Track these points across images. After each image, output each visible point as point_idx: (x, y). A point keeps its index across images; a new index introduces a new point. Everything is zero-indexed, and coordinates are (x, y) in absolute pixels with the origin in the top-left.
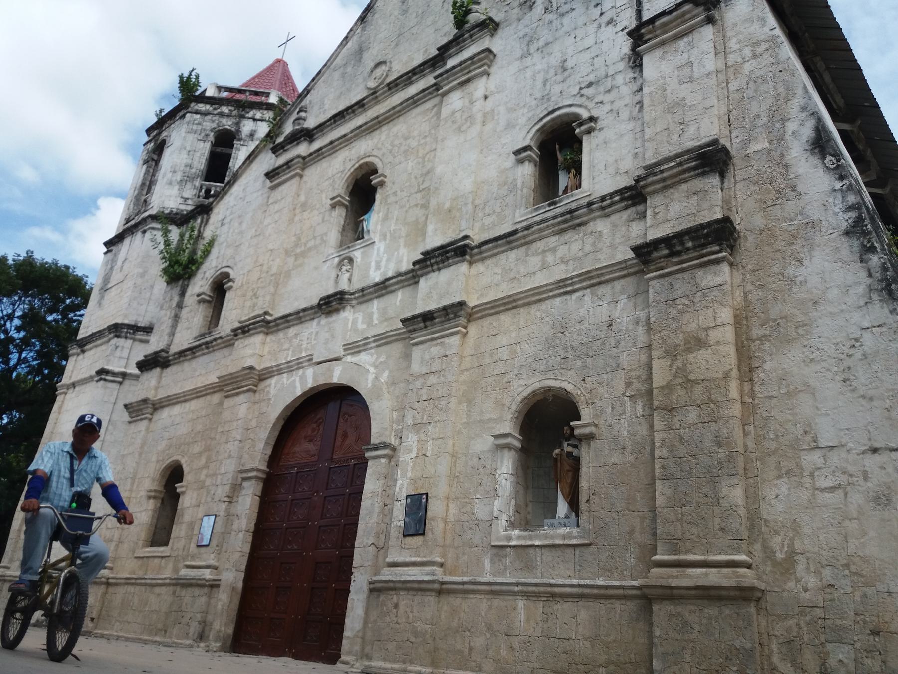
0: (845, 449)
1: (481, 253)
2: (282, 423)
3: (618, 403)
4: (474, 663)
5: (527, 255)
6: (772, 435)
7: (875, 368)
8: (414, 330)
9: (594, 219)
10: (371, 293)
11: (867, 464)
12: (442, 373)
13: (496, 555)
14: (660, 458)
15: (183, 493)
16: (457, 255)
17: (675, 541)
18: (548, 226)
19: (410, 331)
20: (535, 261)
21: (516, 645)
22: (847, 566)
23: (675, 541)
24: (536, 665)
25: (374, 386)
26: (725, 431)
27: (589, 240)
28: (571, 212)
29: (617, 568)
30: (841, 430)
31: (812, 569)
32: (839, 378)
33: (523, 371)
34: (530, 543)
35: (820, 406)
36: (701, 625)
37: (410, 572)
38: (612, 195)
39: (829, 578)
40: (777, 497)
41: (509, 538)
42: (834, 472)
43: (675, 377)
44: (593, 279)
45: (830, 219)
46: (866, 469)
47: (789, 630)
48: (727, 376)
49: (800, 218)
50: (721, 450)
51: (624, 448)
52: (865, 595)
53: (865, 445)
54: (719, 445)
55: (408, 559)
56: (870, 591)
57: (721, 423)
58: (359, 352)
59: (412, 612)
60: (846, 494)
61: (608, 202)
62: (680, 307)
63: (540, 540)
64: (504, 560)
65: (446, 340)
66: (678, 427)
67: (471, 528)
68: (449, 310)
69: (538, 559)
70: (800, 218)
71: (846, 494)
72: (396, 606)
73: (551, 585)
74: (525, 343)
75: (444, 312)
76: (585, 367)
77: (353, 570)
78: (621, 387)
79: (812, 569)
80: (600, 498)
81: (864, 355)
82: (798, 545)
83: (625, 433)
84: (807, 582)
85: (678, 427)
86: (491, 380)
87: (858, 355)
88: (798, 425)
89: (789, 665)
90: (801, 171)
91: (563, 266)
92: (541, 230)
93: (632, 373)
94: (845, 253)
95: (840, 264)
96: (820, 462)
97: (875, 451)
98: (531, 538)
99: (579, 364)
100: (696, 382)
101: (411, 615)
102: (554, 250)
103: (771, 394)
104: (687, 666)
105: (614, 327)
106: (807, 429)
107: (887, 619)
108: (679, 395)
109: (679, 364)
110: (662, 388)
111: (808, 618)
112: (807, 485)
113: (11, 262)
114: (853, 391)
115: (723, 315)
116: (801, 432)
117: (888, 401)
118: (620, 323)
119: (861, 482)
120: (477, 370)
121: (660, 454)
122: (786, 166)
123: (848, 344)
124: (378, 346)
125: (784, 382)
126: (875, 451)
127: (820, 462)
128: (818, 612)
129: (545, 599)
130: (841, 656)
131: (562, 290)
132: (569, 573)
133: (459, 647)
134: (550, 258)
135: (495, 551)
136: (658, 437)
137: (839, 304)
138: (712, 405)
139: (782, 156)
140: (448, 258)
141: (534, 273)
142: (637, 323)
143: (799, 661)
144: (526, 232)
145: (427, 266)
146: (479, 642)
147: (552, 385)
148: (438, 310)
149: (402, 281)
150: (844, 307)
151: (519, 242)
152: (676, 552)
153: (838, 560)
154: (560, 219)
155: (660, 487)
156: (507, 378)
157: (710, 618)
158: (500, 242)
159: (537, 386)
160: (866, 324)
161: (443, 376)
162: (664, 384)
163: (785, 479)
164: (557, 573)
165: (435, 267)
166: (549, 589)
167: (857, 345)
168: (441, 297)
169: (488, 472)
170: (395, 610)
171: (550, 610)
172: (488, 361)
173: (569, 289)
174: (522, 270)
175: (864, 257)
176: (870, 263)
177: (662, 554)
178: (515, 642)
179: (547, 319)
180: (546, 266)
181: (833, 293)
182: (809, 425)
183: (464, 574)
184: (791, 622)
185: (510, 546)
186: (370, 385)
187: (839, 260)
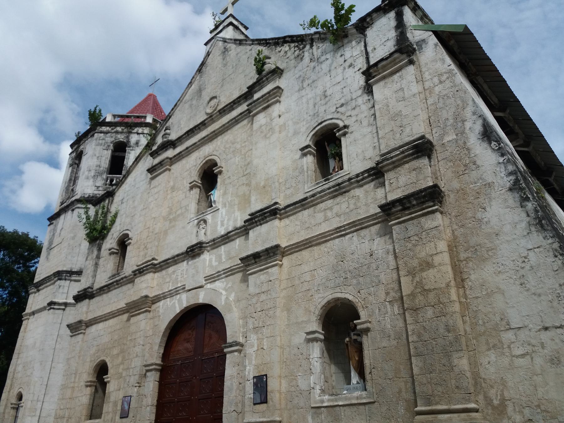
1: (286, 212)
3: (382, 306)
5: (315, 213)
6: (481, 322)
7: (539, 275)
8: (249, 265)
9: (354, 188)
10: (219, 242)
12: (269, 292)
13: (315, 413)
14: (413, 342)
16: (271, 215)
17: (428, 397)
18: (325, 194)
20: (320, 216)
23: (428, 397)
25: (226, 303)
26: (451, 322)
27: (352, 201)
28: (339, 184)
30: (524, 316)
32: (518, 283)
33: (321, 288)
34: (336, 404)
35: (508, 301)
38: (363, 173)
41: (322, 401)
43: (416, 288)
44: (357, 226)
45: (499, 181)
46: (542, 341)
48: (448, 285)
50: (450, 335)
51: (389, 336)
53: (540, 325)
57: (448, 316)
58: (215, 281)
60: (532, 358)
61: (361, 177)
62: (413, 242)
63: (342, 401)
65: (270, 270)
68: (270, 251)
69: (342, 414)
70: (481, 181)
71: (532, 358)
75: (266, 252)
76: (359, 283)
78: (383, 295)
79: (517, 410)
80: (378, 371)
81: (531, 267)
83: (389, 326)
85: (422, 321)
86: (300, 295)
87: (528, 267)
90: (477, 152)
91: (338, 219)
92: (322, 197)
93: (389, 286)
94: (511, 202)
95: (509, 209)
97: (546, 329)
98: (336, 400)
99: (355, 281)
100: (429, 290)
102: (331, 209)
105: (374, 256)
108: (420, 300)
110: (409, 295)
112: (507, 354)
116: (498, 319)
117: (550, 296)
118: (377, 254)
119: (541, 350)
120: (291, 289)
122: (468, 149)
123: (521, 260)
124: (227, 277)
125: (484, 287)
126: (546, 329)
131: (339, 234)
134: (329, 214)
135: (314, 410)
136: (410, 328)
137: (512, 235)
138: (441, 305)
139: (465, 143)
140: (266, 217)
142: (388, 253)
144: (312, 198)
145: (253, 223)
148: (263, 251)
149: (238, 233)
150: (515, 236)
151: (309, 205)
153: (532, 403)
154: (333, 189)
155: (415, 361)
158: (297, 205)
159: (330, 297)
160: (530, 247)
162: (410, 292)
165: (258, 223)
167: (526, 260)
169: (305, 357)
172: (297, 282)
173: (343, 233)
176: (527, 208)
177: (421, 406)
179: (331, 253)
182: (503, 314)
186: (223, 303)
187: (508, 207)
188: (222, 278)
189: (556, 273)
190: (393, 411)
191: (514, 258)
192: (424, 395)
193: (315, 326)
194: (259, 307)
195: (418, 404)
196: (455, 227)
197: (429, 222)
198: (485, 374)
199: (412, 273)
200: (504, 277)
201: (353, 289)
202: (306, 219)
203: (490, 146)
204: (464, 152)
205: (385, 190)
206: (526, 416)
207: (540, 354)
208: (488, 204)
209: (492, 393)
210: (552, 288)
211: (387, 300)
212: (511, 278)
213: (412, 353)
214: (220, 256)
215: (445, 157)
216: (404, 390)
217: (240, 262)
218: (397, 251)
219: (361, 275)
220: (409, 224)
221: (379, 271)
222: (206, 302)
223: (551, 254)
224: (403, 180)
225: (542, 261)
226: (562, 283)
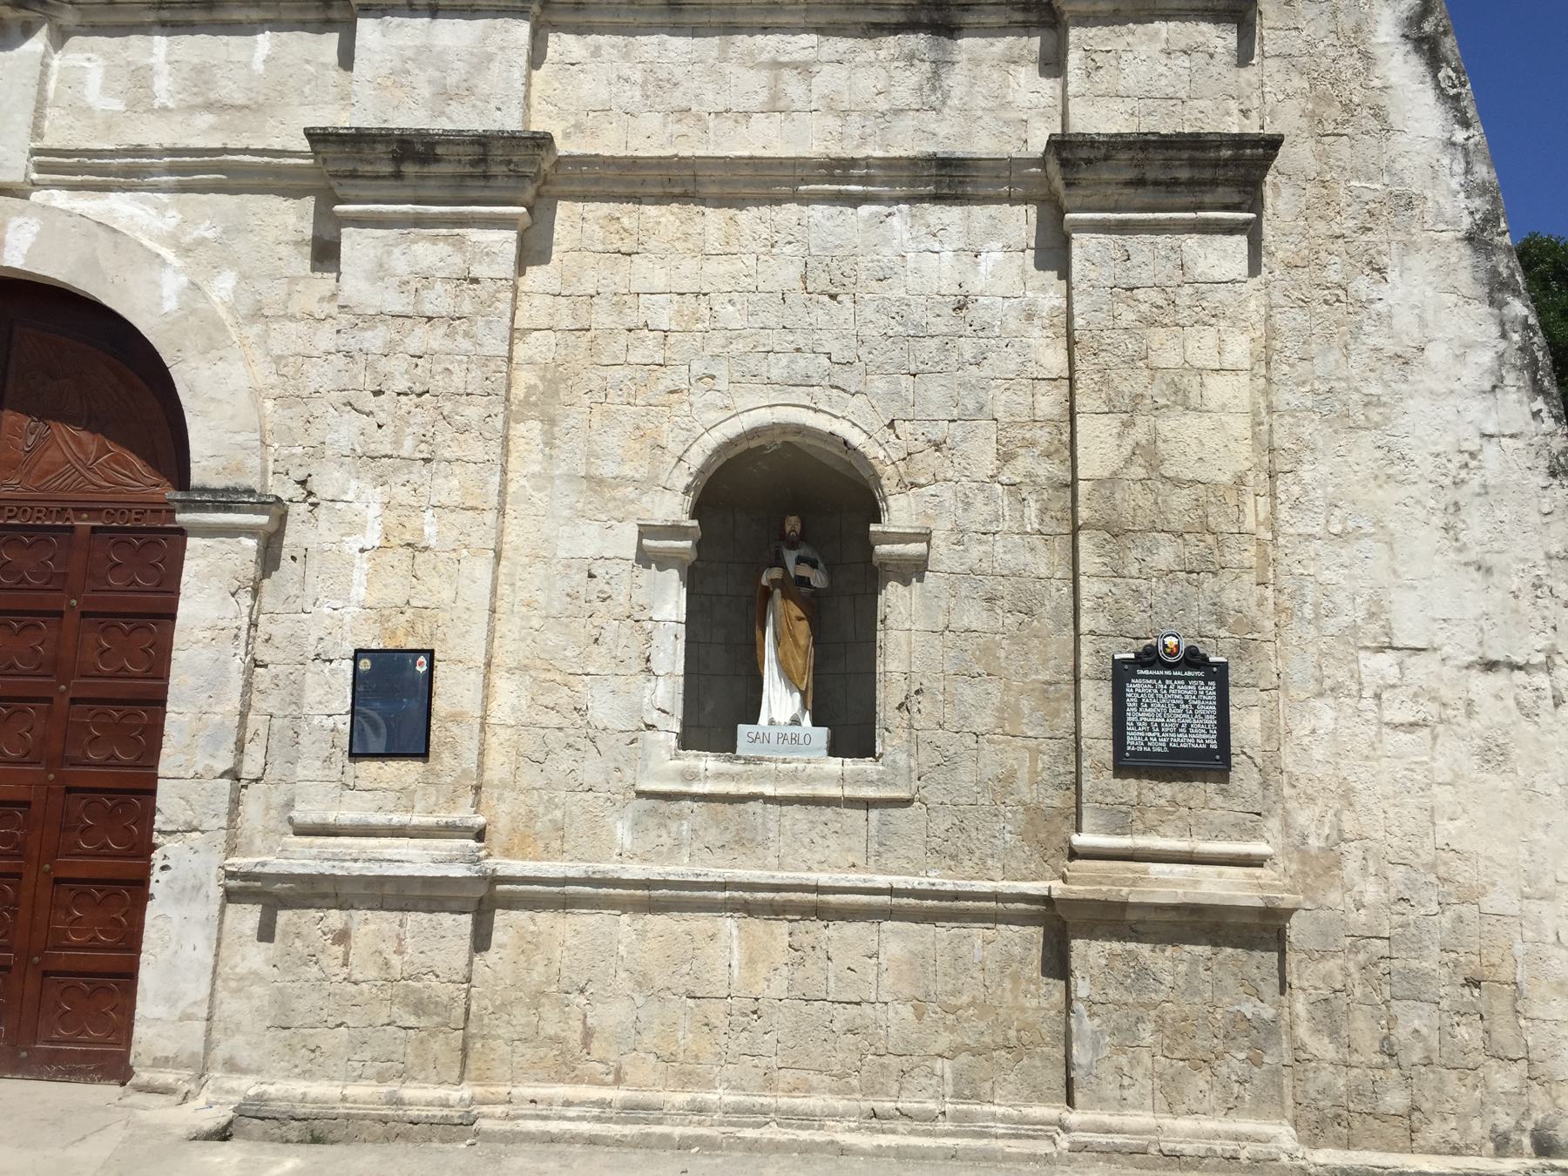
0: (1438, 656)
4: (600, 1068)
6: (1308, 611)
7: (1500, 515)
8: (353, 175)
11: (1474, 689)
14: (1092, 632)
17: (1124, 808)
19: (335, 175)
21: (719, 1020)
22: (1432, 867)
23: (1124, 808)
24: (775, 1061)
26: (1234, 595)
29: (971, 852)
30: (1435, 620)
31: (1372, 870)
32: (1438, 520)
35: (1401, 569)
36: (1175, 974)
37: (388, 854)
39: (1401, 888)
40: (1313, 731)
42: (1416, 695)
43: (1128, 461)
44: (947, 180)
45: (1442, 201)
46: (1471, 696)
47: (1327, 978)
48: (1240, 481)
49: (1386, 180)
50: (1223, 633)
52: (1460, 919)
53: (1473, 653)
55: (378, 819)
56: (1467, 911)
57: (1226, 576)
59: (400, 952)
60: (1435, 738)
62: (1144, 308)
64: (674, 826)
65: (474, 235)
70: (1386, 180)
71: (1435, 738)
72: (342, 937)
73: (818, 889)
74: (725, 298)
75: (478, 149)
76: (895, 395)
77: (157, 839)
79: (1372, 870)
80: (934, 702)
81: (1485, 486)
82: (1348, 825)
84: (1362, 893)
85: (1135, 573)
86: (618, 373)
87: (1474, 484)
88: (1359, 600)
89: (1326, 1040)
90: (1394, 79)
91: (832, 123)
94: (1464, 278)
95: (1454, 298)
96: (1392, 674)
97: (1490, 666)
99: (879, 384)
100: (1177, 483)
101: (396, 960)
103: (1310, 530)
104: (1145, 1057)
105: (970, 313)
106: (1373, 609)
107: (1495, 959)
108: (1133, 501)
109: (1139, 433)
110: (1100, 482)
111: (1362, 957)
112: (1370, 715)
114: (1460, 550)
115: (1238, 350)
116: (1362, 614)
117: (1516, 579)
119: (1462, 719)
121: (1092, 626)
122: (1366, 56)
123: (1459, 459)
125: (1337, 512)
126: (1490, 666)
127: (1392, 674)
128: (1380, 947)
130: (1417, 1024)
132: (851, 859)
133: (551, 1029)
134: (793, 87)
136: (1088, 587)
137: (1448, 378)
138: (1209, 539)
139: (1358, 30)
141: (747, 114)
142: (1030, 317)
143: (1344, 1034)
146: (611, 1015)
147: (809, 423)
150: (1457, 386)
153: (1418, 855)
155: (1092, 694)
156: (678, 377)
159: (764, 417)
160: (1490, 429)
161: (466, 334)
162: (1106, 474)
163: (1330, 701)
164: (818, 857)
166: (812, 897)
167: (1473, 464)
168: (445, 95)
170: (338, 950)
171: (807, 940)
172: (602, 317)
174: (709, 96)
175: (1498, 296)
176: (1505, 311)
177: (1093, 832)
178: (715, 1013)
179: (788, 249)
180: (781, 104)
181: (1437, 354)
182: (1378, 603)
183: (548, 853)
184: (1332, 965)
185: (695, 797)
186: (170, 305)
187: (1454, 290)
188: (156, 188)
189: (1546, 519)
190: (974, 834)
191: (1440, 449)
192: (1109, 800)
193: (673, 507)
194: (399, 375)
195: (1084, 826)
196: (1278, 298)
197: (1212, 259)
198: (1297, 762)
199: (1128, 409)
200: (1402, 493)
201: (868, 409)
202: (679, 73)
203: (1435, 77)
204: (1349, 61)
205: (1065, 86)
206: (1393, 890)
207: (1459, 730)
208: (1396, 260)
209: (1303, 818)
210: (1525, 560)
211: (1003, 479)
212: (1419, 502)
213: (1084, 668)
214: (141, 77)
215: (1286, 51)
216: (1023, 774)
217: (305, 145)
218: (1079, 322)
219: (913, 370)
220: (1139, 244)
221: (986, 371)
223: (1543, 463)
224: (1172, 75)
225: (1514, 477)
226: (1556, 548)
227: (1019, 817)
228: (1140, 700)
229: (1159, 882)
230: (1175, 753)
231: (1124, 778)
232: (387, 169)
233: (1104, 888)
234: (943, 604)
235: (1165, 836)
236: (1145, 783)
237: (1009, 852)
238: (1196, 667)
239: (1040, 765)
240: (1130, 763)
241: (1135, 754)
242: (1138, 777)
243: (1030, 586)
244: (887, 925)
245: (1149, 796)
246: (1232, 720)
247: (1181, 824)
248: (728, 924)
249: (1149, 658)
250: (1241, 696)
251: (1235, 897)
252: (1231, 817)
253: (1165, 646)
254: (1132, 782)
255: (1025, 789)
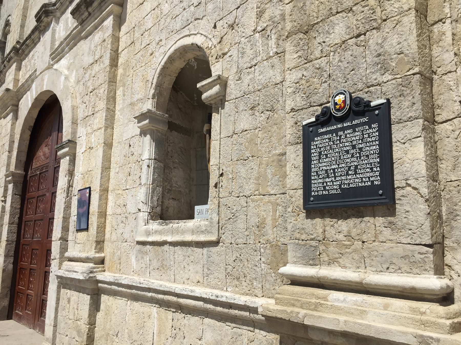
2: (28, 133)
15: (2, 197)
17: (314, 243)
23: (314, 243)
25: (64, 86)
50: (387, 77)
54: (385, 69)
66: (317, 53)
67: (122, 222)
113: (154, 110)
121: (293, 105)
129: (174, 310)
135: (139, 247)
152: (313, 261)
157: (353, 28)
169: (135, 158)
177: (295, 263)
192: (304, 237)
216: (269, 221)
222: (49, 89)
227: (268, 251)
228: (320, 153)
229: (336, 310)
230: (347, 193)
231: (313, 218)
232: (86, 14)
233: (289, 309)
234: (232, 119)
235: (344, 267)
236: (328, 221)
237: (264, 276)
238: (361, 114)
239: (278, 214)
240: (317, 205)
241: (317, 198)
242: (322, 217)
243: (272, 91)
244: (207, 320)
245: (331, 233)
246: (396, 155)
247: (356, 257)
248: (154, 310)
249: (326, 118)
250: (405, 131)
251: (390, 331)
252: (400, 250)
253: (336, 104)
254: (318, 221)
255: (270, 232)
